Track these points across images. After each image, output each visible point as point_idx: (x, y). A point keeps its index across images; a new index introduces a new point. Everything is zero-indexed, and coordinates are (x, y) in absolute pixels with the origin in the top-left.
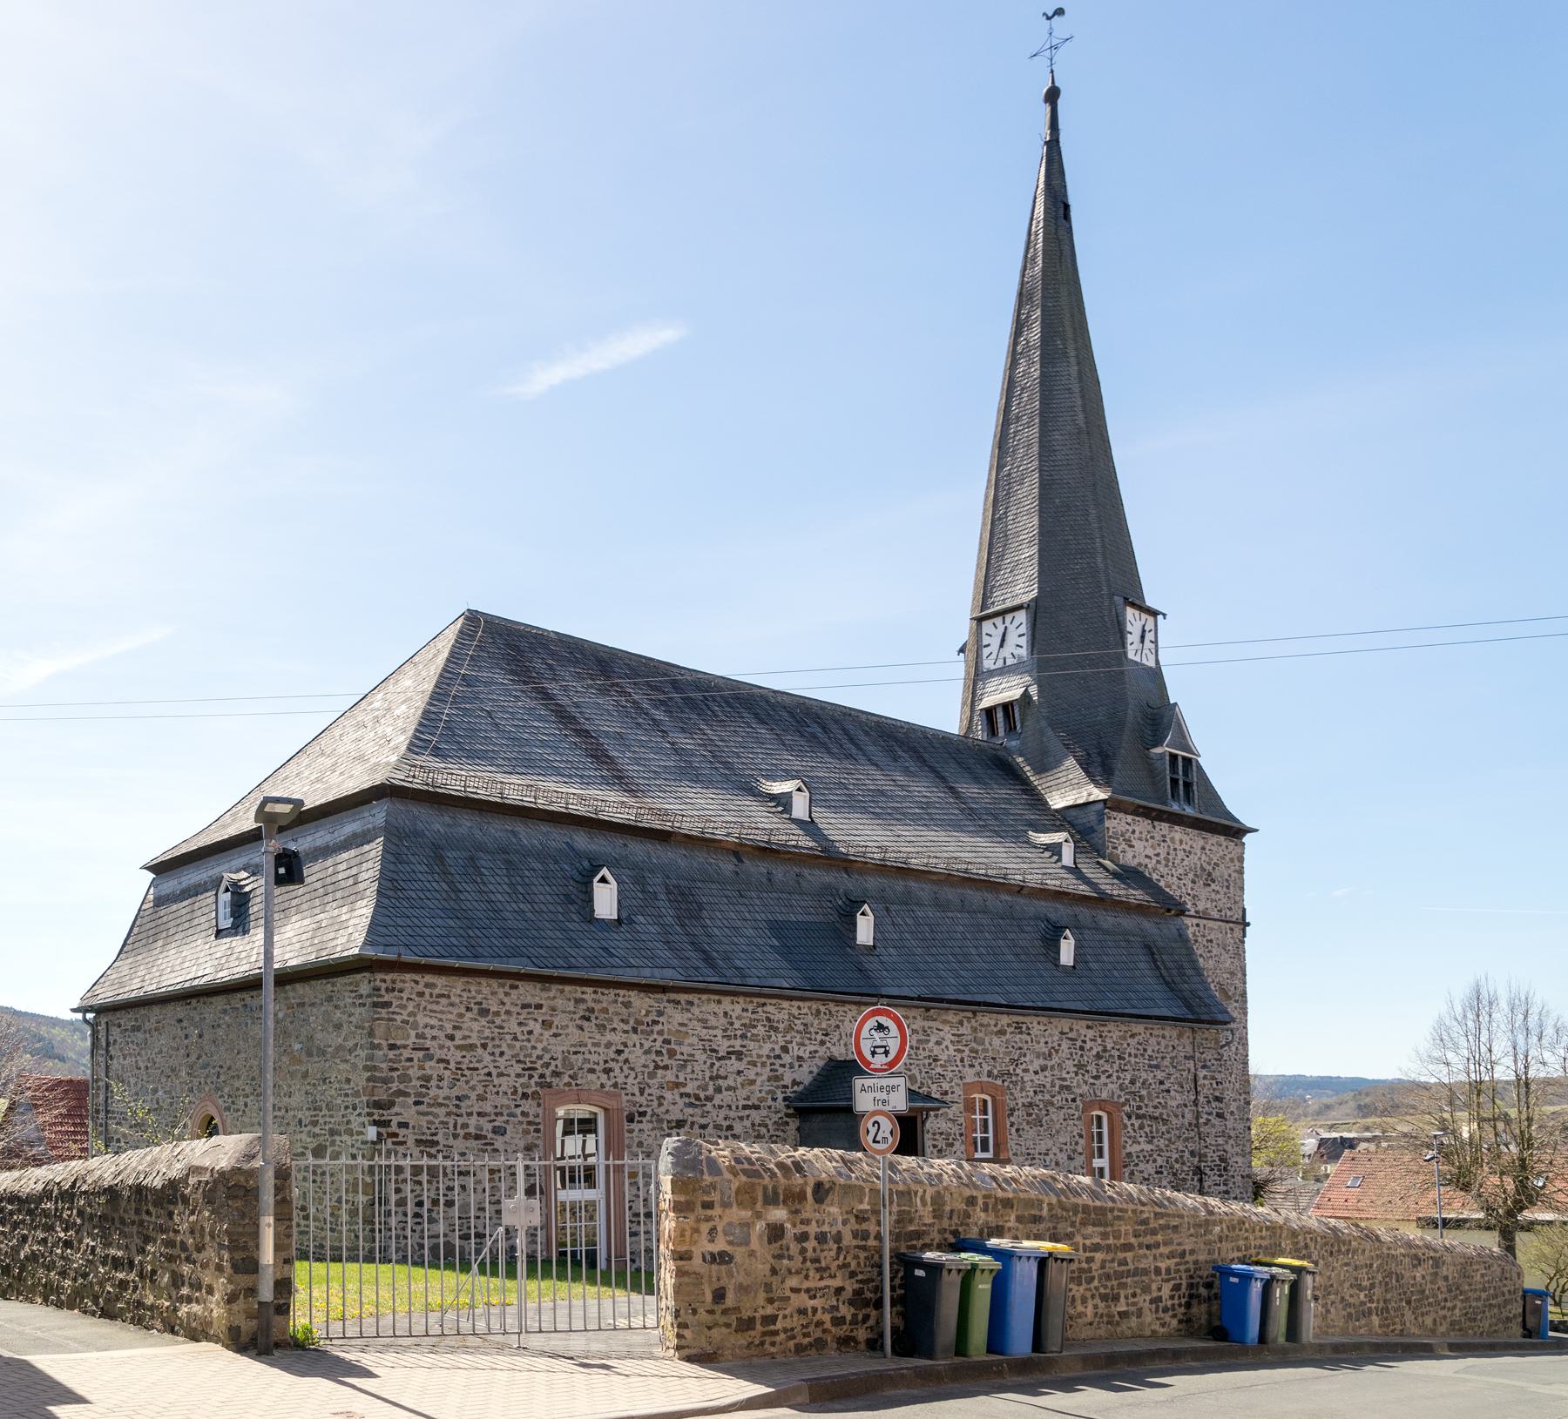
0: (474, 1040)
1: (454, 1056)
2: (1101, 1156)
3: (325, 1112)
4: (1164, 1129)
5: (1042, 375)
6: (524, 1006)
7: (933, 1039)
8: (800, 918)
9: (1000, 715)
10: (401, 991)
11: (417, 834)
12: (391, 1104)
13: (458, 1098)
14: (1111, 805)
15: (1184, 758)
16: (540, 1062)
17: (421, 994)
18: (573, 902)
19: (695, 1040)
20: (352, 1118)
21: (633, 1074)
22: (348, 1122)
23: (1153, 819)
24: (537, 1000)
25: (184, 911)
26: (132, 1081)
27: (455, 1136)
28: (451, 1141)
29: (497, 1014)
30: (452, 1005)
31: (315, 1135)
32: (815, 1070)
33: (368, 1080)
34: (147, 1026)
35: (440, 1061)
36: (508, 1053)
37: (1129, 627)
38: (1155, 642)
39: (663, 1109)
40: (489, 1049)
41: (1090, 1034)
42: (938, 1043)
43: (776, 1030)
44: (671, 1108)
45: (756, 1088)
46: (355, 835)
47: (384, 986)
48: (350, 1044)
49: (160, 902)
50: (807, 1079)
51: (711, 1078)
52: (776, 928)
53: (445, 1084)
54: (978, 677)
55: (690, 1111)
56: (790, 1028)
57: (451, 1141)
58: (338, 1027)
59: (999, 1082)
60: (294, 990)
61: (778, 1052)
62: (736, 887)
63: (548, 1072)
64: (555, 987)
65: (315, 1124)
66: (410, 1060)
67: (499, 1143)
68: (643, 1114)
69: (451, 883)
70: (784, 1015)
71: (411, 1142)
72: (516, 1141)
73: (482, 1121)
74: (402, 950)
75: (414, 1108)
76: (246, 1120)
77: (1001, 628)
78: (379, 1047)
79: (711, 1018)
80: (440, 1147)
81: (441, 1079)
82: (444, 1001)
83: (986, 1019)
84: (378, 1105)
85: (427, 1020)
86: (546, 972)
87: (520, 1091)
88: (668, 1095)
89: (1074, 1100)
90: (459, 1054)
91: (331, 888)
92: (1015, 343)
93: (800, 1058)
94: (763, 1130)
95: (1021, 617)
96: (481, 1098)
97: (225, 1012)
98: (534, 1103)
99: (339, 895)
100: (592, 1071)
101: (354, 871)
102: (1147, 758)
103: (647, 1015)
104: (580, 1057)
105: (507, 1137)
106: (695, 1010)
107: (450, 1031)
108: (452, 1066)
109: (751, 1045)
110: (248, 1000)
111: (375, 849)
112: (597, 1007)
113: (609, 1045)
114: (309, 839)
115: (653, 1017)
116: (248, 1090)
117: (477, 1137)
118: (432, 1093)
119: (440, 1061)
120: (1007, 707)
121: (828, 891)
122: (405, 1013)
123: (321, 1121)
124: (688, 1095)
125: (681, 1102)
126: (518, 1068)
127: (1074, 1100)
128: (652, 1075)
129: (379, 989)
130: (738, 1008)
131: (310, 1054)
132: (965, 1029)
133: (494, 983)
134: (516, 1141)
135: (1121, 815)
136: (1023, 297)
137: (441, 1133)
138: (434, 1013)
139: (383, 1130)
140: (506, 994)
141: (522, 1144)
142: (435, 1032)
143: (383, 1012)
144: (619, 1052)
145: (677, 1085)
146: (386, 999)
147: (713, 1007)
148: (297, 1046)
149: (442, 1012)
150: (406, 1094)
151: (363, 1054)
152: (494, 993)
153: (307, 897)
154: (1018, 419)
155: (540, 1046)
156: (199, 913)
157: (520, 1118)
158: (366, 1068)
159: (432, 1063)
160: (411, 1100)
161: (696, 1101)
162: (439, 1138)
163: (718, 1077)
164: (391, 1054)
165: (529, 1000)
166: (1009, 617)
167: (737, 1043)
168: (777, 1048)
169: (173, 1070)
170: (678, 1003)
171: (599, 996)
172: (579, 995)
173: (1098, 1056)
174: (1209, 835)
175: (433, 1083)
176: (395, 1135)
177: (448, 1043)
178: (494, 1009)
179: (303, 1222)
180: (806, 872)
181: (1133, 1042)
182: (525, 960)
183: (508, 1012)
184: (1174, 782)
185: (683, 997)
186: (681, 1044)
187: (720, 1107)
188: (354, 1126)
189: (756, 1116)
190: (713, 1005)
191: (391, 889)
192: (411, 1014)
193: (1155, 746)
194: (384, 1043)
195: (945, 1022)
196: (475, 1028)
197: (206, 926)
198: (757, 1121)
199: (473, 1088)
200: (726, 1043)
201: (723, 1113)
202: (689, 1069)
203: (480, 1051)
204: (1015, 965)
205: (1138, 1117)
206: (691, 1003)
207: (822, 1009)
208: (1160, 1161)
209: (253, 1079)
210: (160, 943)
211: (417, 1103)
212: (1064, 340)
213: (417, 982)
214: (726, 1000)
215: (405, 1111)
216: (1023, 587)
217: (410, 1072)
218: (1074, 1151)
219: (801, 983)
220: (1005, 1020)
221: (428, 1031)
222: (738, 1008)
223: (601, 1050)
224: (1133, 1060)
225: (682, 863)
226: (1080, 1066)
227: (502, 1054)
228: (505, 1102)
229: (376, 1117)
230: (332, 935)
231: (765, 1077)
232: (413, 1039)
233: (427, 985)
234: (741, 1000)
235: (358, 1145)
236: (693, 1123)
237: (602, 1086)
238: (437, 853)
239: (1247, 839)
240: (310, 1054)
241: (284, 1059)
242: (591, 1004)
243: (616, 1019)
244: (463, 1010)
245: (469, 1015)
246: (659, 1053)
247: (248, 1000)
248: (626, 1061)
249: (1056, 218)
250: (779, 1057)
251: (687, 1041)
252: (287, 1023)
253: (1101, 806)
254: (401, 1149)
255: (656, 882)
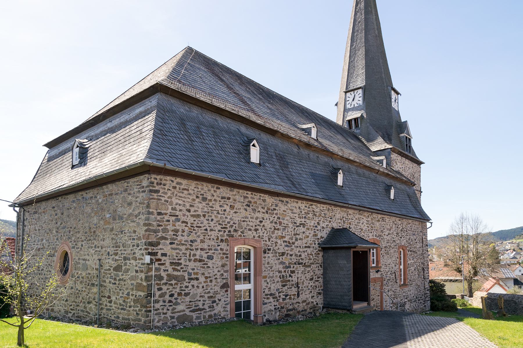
0: (199, 213)
1: (190, 220)
3: (121, 248)
7: (361, 222)
8: (320, 173)
9: (353, 122)
10: (165, 185)
11: (173, 112)
12: (158, 244)
13: (191, 241)
14: (393, 150)
16: (229, 225)
17: (175, 188)
18: (241, 154)
19: (288, 218)
20: (136, 251)
21: (266, 232)
22: (134, 253)
24: (228, 195)
25: (59, 161)
26: (33, 236)
27: (190, 260)
28: (188, 263)
29: (210, 200)
30: (189, 194)
31: (116, 260)
32: (328, 232)
33: (146, 231)
34: (40, 211)
35: (183, 222)
36: (215, 220)
39: (277, 248)
40: (207, 218)
41: (400, 222)
42: (362, 224)
43: (316, 215)
46: (141, 113)
47: (155, 181)
48: (136, 212)
49: (50, 159)
50: (325, 236)
52: (313, 175)
53: (185, 234)
54: (346, 110)
55: (286, 248)
57: (188, 263)
58: (130, 204)
60: (107, 188)
61: (316, 224)
63: (232, 230)
64: (236, 190)
65: (116, 254)
66: (168, 221)
68: (269, 250)
69: (189, 137)
70: (318, 210)
71: (168, 264)
72: (218, 262)
73: (203, 253)
74: (166, 162)
75: (170, 246)
76: (82, 253)
77: (353, 95)
78: (152, 213)
80: (182, 266)
81: (183, 231)
82: (185, 192)
83: (375, 215)
84: (151, 244)
85: (177, 201)
87: (220, 238)
88: (279, 241)
90: (192, 219)
91: (127, 138)
92: (356, 9)
93: (323, 227)
94: (311, 257)
95: (360, 91)
96: (202, 241)
97: (74, 201)
98: (226, 244)
99: (132, 140)
100: (250, 230)
101: (140, 128)
103: (271, 206)
104: (245, 223)
105: (214, 261)
106: (289, 205)
107: (188, 208)
108: (189, 225)
109: (308, 221)
110: (85, 195)
111: (152, 117)
112: (253, 201)
113: (257, 218)
114: (118, 120)
115: (274, 207)
116: (83, 238)
117: (200, 261)
118: (179, 238)
119: (183, 222)
120: (356, 120)
121: (326, 164)
122: (166, 196)
123: (120, 253)
124: (286, 242)
125: (283, 244)
128: (273, 233)
129: (153, 183)
130: (303, 205)
131: (114, 219)
132: (369, 219)
133: (210, 185)
134: (218, 262)
137: (183, 258)
138: (180, 198)
139: (153, 258)
140: (215, 191)
141: (220, 264)
143: (155, 195)
144: (261, 222)
145: (282, 237)
146: (157, 188)
147: (295, 204)
148: (108, 216)
150: (166, 239)
151: (143, 217)
152: (209, 190)
153: (116, 144)
154: (358, 31)
155: (229, 217)
156: (66, 160)
157: (220, 251)
158: (145, 225)
159: (180, 223)
160: (168, 242)
161: (289, 244)
162: (182, 261)
163: (297, 234)
164: (159, 218)
165: (224, 195)
166: (356, 91)
167: (303, 220)
168: (316, 223)
169: (50, 230)
170: (283, 201)
172: (245, 195)
175: (180, 233)
176: (160, 260)
177: (188, 213)
179: (108, 304)
180: (320, 156)
183: (215, 200)
184: (407, 145)
185: (285, 199)
186: (284, 219)
187: (297, 247)
188: (138, 255)
189: (309, 251)
190: (295, 203)
191: (159, 133)
194: (155, 212)
195: (364, 216)
196: (200, 207)
197: (68, 165)
198: (309, 253)
199: (199, 236)
201: (298, 249)
202: (287, 230)
203: (202, 218)
204: (380, 197)
206: (287, 202)
207: (330, 208)
209: (86, 233)
210: (48, 175)
211: (171, 243)
213: (172, 181)
214: (300, 202)
215: (165, 247)
216: (360, 81)
217: (168, 227)
219: (325, 197)
220: (380, 216)
221: (178, 207)
222: (303, 205)
223: (254, 220)
226: (397, 234)
227: (212, 220)
228: (213, 243)
229: (150, 251)
230: (128, 158)
231: (312, 235)
232: (170, 210)
233: (178, 183)
234: (304, 202)
235: (140, 265)
236: (288, 254)
237: (254, 237)
238: (182, 122)
239: (422, 166)
240: (114, 219)
241: (101, 222)
242: (250, 199)
243: (260, 207)
244: (195, 198)
245: (197, 200)
246: (276, 223)
247: (85, 195)
248: (264, 226)
250: (316, 227)
252: (103, 204)
253: (390, 150)
254: (163, 267)
255: (271, 151)
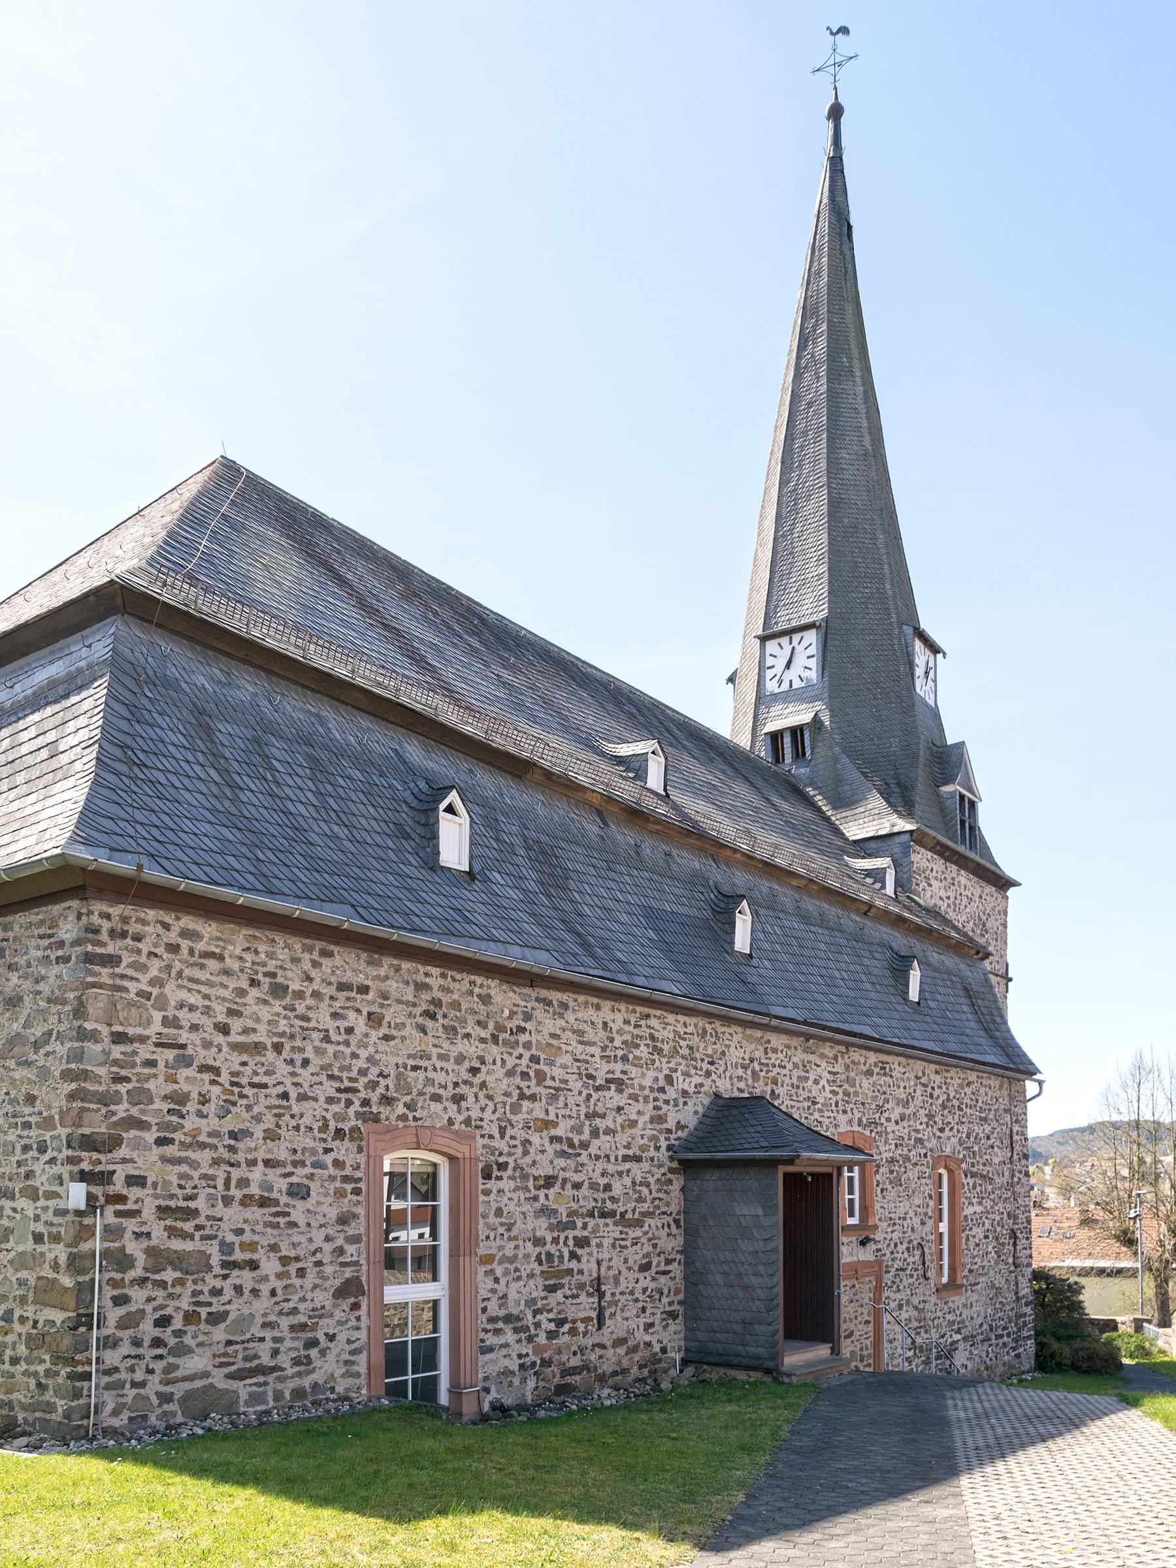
0: (261, 1036)
2: (852, 1215)
4: (990, 1188)
5: (829, 390)
6: (342, 987)
9: (787, 740)
10: (138, 938)
11: (169, 684)
12: (115, 1142)
13: (233, 1135)
15: (969, 799)
16: (363, 1080)
17: (174, 948)
18: (407, 837)
19: (567, 1059)
20: (37, 1167)
22: (29, 1175)
23: (947, 859)
24: (360, 979)
27: (227, 1201)
28: (219, 1210)
29: (300, 995)
30: (226, 972)
32: (700, 1110)
33: (72, 1097)
35: (204, 1068)
36: (316, 1061)
37: (917, 661)
38: (935, 681)
39: (528, 1160)
40: (286, 1054)
42: (816, 1082)
43: (660, 1051)
44: (539, 1157)
45: (637, 1131)
46: (53, 684)
47: (106, 925)
48: (37, 1031)
50: (692, 1121)
51: (587, 1116)
53: (211, 1108)
55: (561, 1162)
56: (675, 1051)
59: (867, 1133)
61: (662, 1083)
62: (604, 856)
63: (374, 1097)
66: (151, 1063)
67: (298, 1213)
68: (503, 1166)
69: (224, 772)
70: (667, 1034)
71: (149, 1213)
72: (324, 1208)
73: (273, 1175)
74: (145, 860)
75: (156, 1151)
78: (94, 1036)
79: (589, 1029)
80: (201, 1220)
81: (204, 1100)
82: (212, 964)
83: (856, 1055)
84: (89, 1143)
85: (183, 995)
86: (382, 932)
87: (332, 1125)
88: (535, 1139)
89: (925, 1155)
90: (236, 1059)
92: (799, 357)
93: (685, 1093)
95: (811, 637)
98: (353, 1146)
99: (20, 778)
100: (436, 1098)
101: (51, 737)
102: (938, 795)
103: (510, 1017)
104: (421, 1074)
105: (312, 1201)
106: (570, 1016)
107: (221, 1018)
108: (225, 1078)
109: (634, 1072)
112: (446, 999)
113: (460, 1059)
115: (518, 1021)
117: (264, 1202)
118: (190, 1123)
119: (204, 1068)
120: (796, 732)
121: (696, 880)
122: (144, 978)
125: (550, 1149)
126: (330, 1088)
127: (925, 1155)
128: (516, 1109)
129: (97, 931)
130: (619, 1018)
133: (297, 944)
134: (324, 1208)
135: (923, 850)
136: (808, 310)
138: (192, 985)
139: (98, 1190)
140: (315, 964)
141: (333, 1214)
142: (196, 1018)
144: (474, 1071)
145: (547, 1124)
146: (110, 949)
149: (209, 983)
150: (142, 1125)
151: (61, 1049)
152: (295, 960)
154: (805, 433)
155: (363, 1054)
157: (332, 1171)
158: (67, 1075)
159: (191, 1072)
160: (150, 1136)
161: (569, 1148)
162: (200, 1204)
163: (595, 1115)
164: (117, 1051)
165: (348, 977)
166: (796, 638)
167: (618, 1067)
168: (661, 1077)
170: (549, 1003)
171: (448, 982)
172: (420, 978)
173: (944, 1106)
174: (984, 884)
175: (192, 1107)
176: (121, 1199)
177: (220, 1039)
178: (295, 986)
181: (968, 1090)
182: (347, 908)
183: (316, 995)
184: (963, 822)
185: (556, 996)
186: (551, 1064)
187: (598, 1158)
188: (41, 1182)
190: (591, 1011)
192: (152, 982)
193: (946, 784)
194: (104, 1030)
195: (822, 1056)
196: (263, 1016)
198: (638, 1179)
199: (258, 1119)
200: (605, 1067)
201: (601, 1165)
203: (271, 1055)
204: (873, 995)
205: (973, 1175)
206: (565, 1006)
207: (708, 1027)
208: (987, 1226)
211: (161, 1142)
212: (850, 358)
213: (166, 927)
214: (607, 1005)
215: (140, 1156)
216: (811, 602)
217: (151, 1085)
218: (926, 1214)
219: (692, 990)
220: (873, 1057)
221: (183, 1014)
222: (619, 1018)
223: (450, 1066)
224: (969, 1111)
225: (539, 808)
226: (930, 1116)
227: (306, 1063)
228: (309, 1143)
229: (85, 1166)
231: (647, 1118)
233: (184, 934)
235: (49, 1216)
236: (565, 1180)
237: (451, 1122)
238: (202, 718)
239: (1011, 892)
242: (437, 994)
243: (471, 1020)
244: (244, 984)
245: (254, 993)
246: (525, 1075)
248: (483, 1085)
249: (840, 234)
250: (662, 1090)
251: (560, 1061)
253: (907, 837)
254: (131, 1225)
255: (511, 829)
